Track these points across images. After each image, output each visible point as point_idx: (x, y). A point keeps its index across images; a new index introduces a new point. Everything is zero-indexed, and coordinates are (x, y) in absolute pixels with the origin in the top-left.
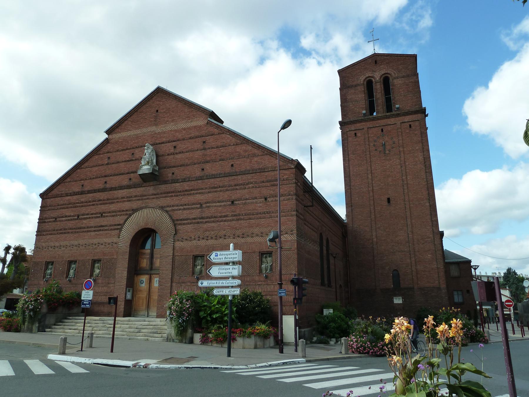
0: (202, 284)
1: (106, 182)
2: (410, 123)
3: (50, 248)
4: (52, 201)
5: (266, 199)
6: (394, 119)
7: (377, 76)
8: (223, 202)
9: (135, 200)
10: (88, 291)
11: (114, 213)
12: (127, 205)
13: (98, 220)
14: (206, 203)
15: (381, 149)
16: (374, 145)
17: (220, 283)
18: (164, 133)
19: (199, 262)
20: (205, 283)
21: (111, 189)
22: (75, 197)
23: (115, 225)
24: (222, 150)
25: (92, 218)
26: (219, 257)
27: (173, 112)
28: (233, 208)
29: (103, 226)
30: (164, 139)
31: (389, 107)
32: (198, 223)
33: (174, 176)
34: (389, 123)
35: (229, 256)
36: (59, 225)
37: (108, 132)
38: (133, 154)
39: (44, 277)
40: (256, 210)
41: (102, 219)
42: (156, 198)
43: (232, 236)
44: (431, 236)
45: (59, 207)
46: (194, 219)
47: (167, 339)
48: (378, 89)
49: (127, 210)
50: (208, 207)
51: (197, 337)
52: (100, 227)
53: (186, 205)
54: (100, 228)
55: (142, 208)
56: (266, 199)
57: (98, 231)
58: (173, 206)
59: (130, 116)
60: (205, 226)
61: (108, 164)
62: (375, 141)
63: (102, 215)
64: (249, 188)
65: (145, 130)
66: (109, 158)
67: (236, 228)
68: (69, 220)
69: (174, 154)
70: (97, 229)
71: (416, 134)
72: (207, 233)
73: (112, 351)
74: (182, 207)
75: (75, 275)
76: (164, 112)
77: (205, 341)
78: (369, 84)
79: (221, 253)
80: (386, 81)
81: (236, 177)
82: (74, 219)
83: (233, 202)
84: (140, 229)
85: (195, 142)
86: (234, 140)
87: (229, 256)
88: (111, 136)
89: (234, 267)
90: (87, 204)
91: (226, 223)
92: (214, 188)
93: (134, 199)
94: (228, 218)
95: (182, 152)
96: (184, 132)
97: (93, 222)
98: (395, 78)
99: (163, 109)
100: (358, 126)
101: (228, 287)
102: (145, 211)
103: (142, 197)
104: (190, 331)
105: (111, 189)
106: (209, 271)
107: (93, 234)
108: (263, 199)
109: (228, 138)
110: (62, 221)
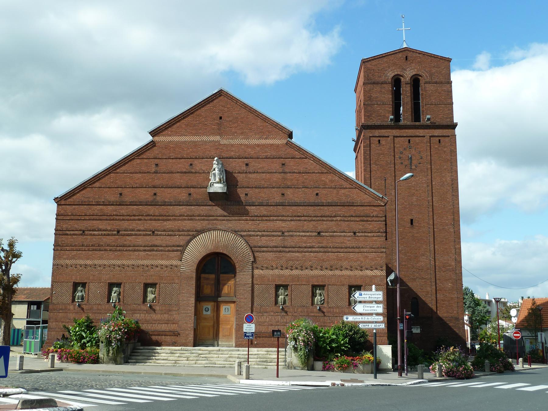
0: (347, 318)
1: (155, 194)
2: (440, 138)
4: (74, 209)
5: (355, 233)
6: (422, 130)
7: (408, 75)
8: (308, 232)
9: (199, 220)
10: (250, 324)
11: (171, 232)
12: (188, 224)
13: (148, 238)
14: (288, 232)
15: (407, 162)
16: (400, 158)
17: (365, 318)
19: (281, 291)
20: (351, 318)
21: (164, 204)
22: (110, 208)
23: (174, 246)
24: (306, 176)
25: (140, 235)
26: (363, 296)
27: (242, 122)
28: (319, 239)
29: (157, 246)
30: (233, 153)
31: (416, 116)
32: (280, 252)
33: (248, 198)
34: (418, 134)
35: (373, 296)
36: (88, 240)
37: (154, 133)
38: (191, 165)
39: (73, 300)
40: (345, 243)
41: (154, 238)
42: (227, 220)
43: (319, 267)
44: (453, 263)
45: (87, 218)
47: (288, 367)
48: (406, 91)
49: (188, 231)
50: (292, 236)
51: (319, 364)
52: (151, 246)
53: (264, 231)
54: (152, 248)
55: (209, 230)
56: (355, 233)
57: (150, 251)
58: (249, 231)
59: (184, 118)
60: (288, 255)
61: (156, 172)
62: (401, 153)
63: (153, 232)
64: (337, 221)
65: (205, 138)
66: (157, 165)
67: (323, 260)
68: (104, 235)
69: (246, 173)
70: (148, 248)
71: (445, 152)
72: (291, 263)
73: (278, 377)
74: (260, 233)
75: (119, 299)
76: (230, 121)
77: (325, 369)
78: (397, 82)
79: (366, 293)
80: (416, 82)
81: (322, 207)
82: (112, 235)
83: (319, 233)
84: (208, 252)
85: (272, 162)
87: (373, 296)
88: (157, 139)
89: (379, 305)
90: (131, 217)
91: (312, 254)
92: (297, 217)
93: (197, 218)
95: (257, 172)
96: (258, 149)
97: (140, 240)
98: (426, 83)
99: (229, 117)
100: (383, 132)
101: (372, 322)
102: (214, 234)
103: (207, 217)
104: (312, 359)
105: (164, 204)
106: (353, 308)
108: (352, 234)
109: (312, 164)
110: (94, 235)
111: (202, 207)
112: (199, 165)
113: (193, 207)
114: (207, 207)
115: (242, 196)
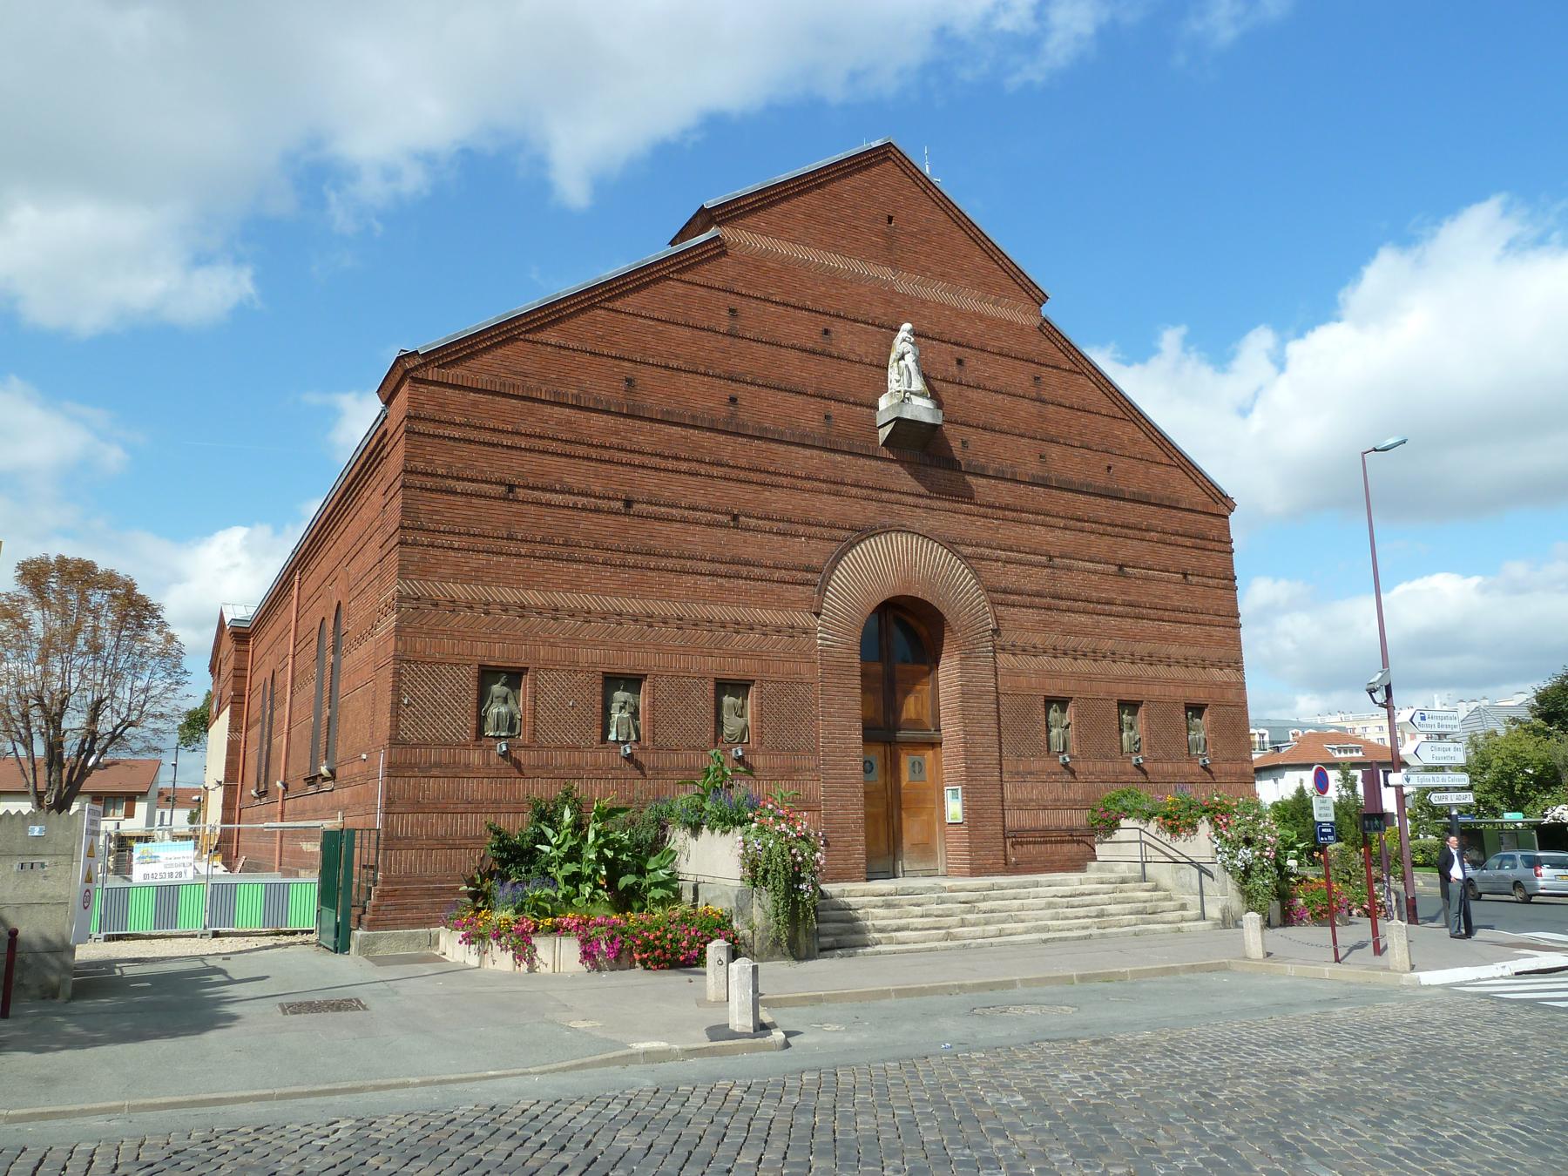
3: (496, 610)
11: (788, 525)
12: (828, 506)
18: (924, 302)
38: (826, 332)
46: (1039, 595)
47: (1224, 921)
54: (734, 567)
55: (886, 530)
60: (1067, 618)
63: (735, 518)
69: (960, 384)
86: (1105, 405)
93: (854, 491)
94: (1114, 608)
97: (698, 539)
102: (900, 541)
107: (706, 583)
111: (861, 461)
112: (847, 339)
113: (838, 457)
114: (873, 463)
115: (955, 445)
